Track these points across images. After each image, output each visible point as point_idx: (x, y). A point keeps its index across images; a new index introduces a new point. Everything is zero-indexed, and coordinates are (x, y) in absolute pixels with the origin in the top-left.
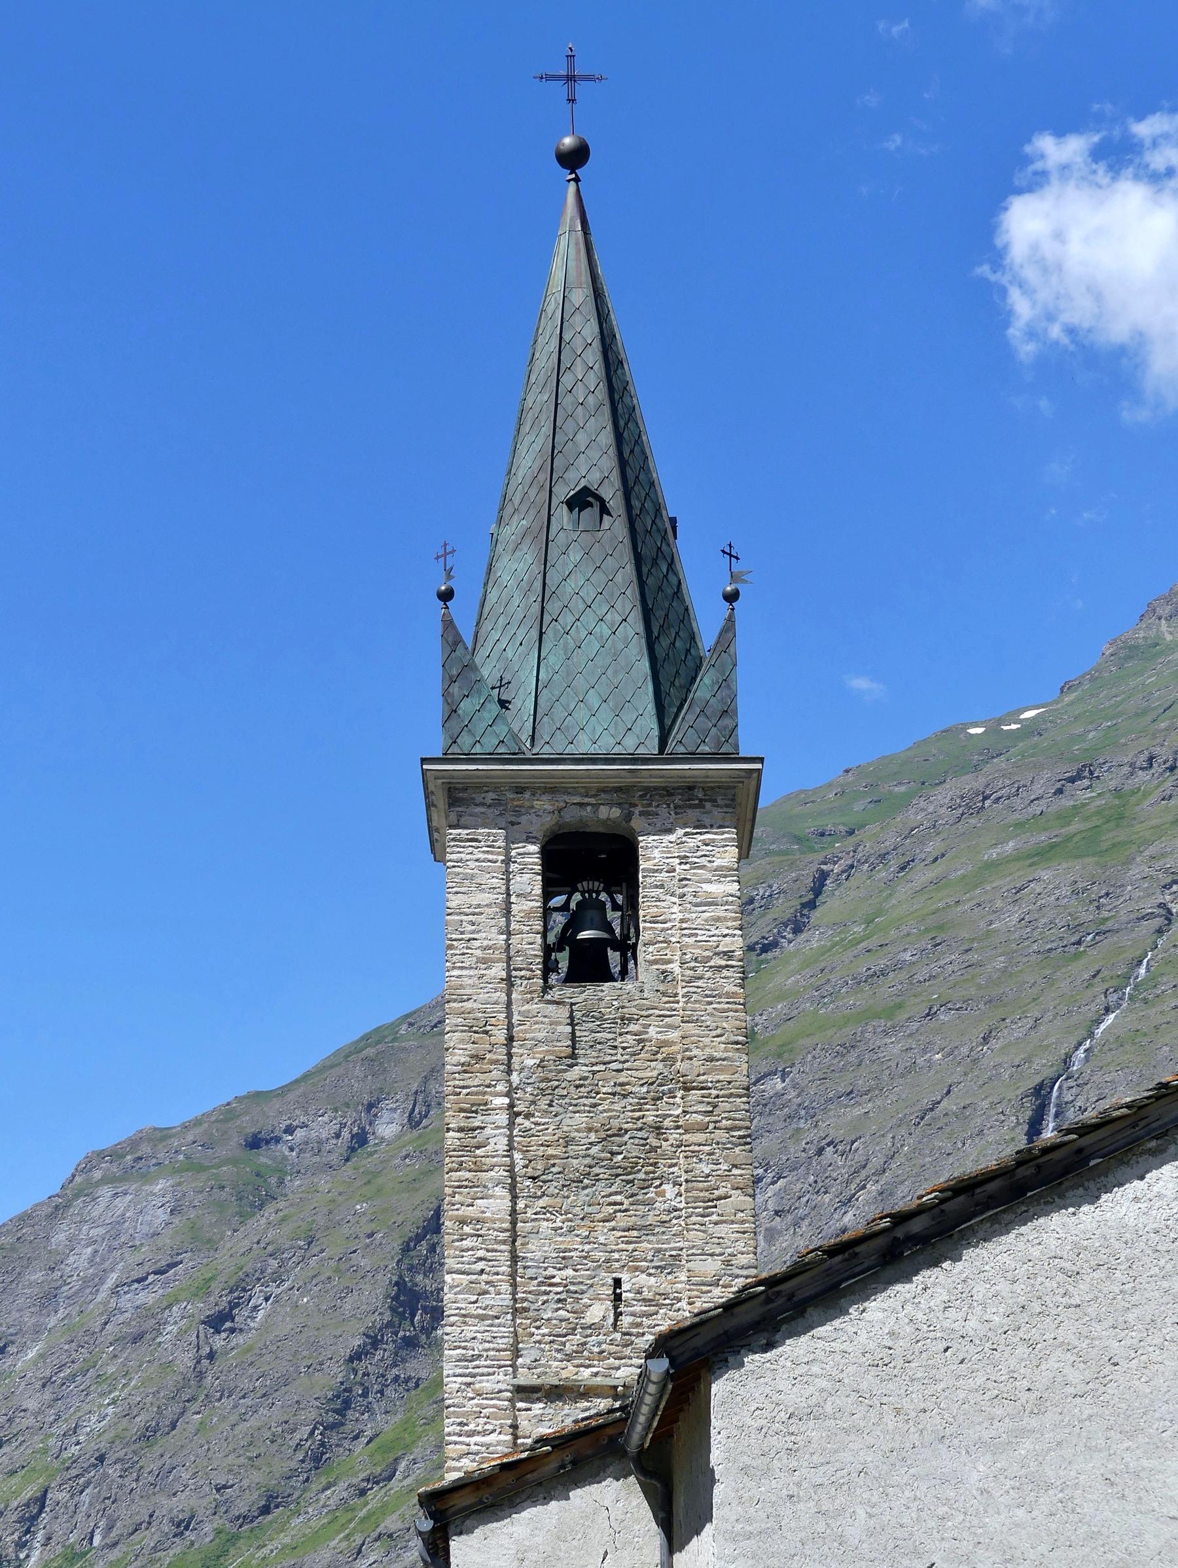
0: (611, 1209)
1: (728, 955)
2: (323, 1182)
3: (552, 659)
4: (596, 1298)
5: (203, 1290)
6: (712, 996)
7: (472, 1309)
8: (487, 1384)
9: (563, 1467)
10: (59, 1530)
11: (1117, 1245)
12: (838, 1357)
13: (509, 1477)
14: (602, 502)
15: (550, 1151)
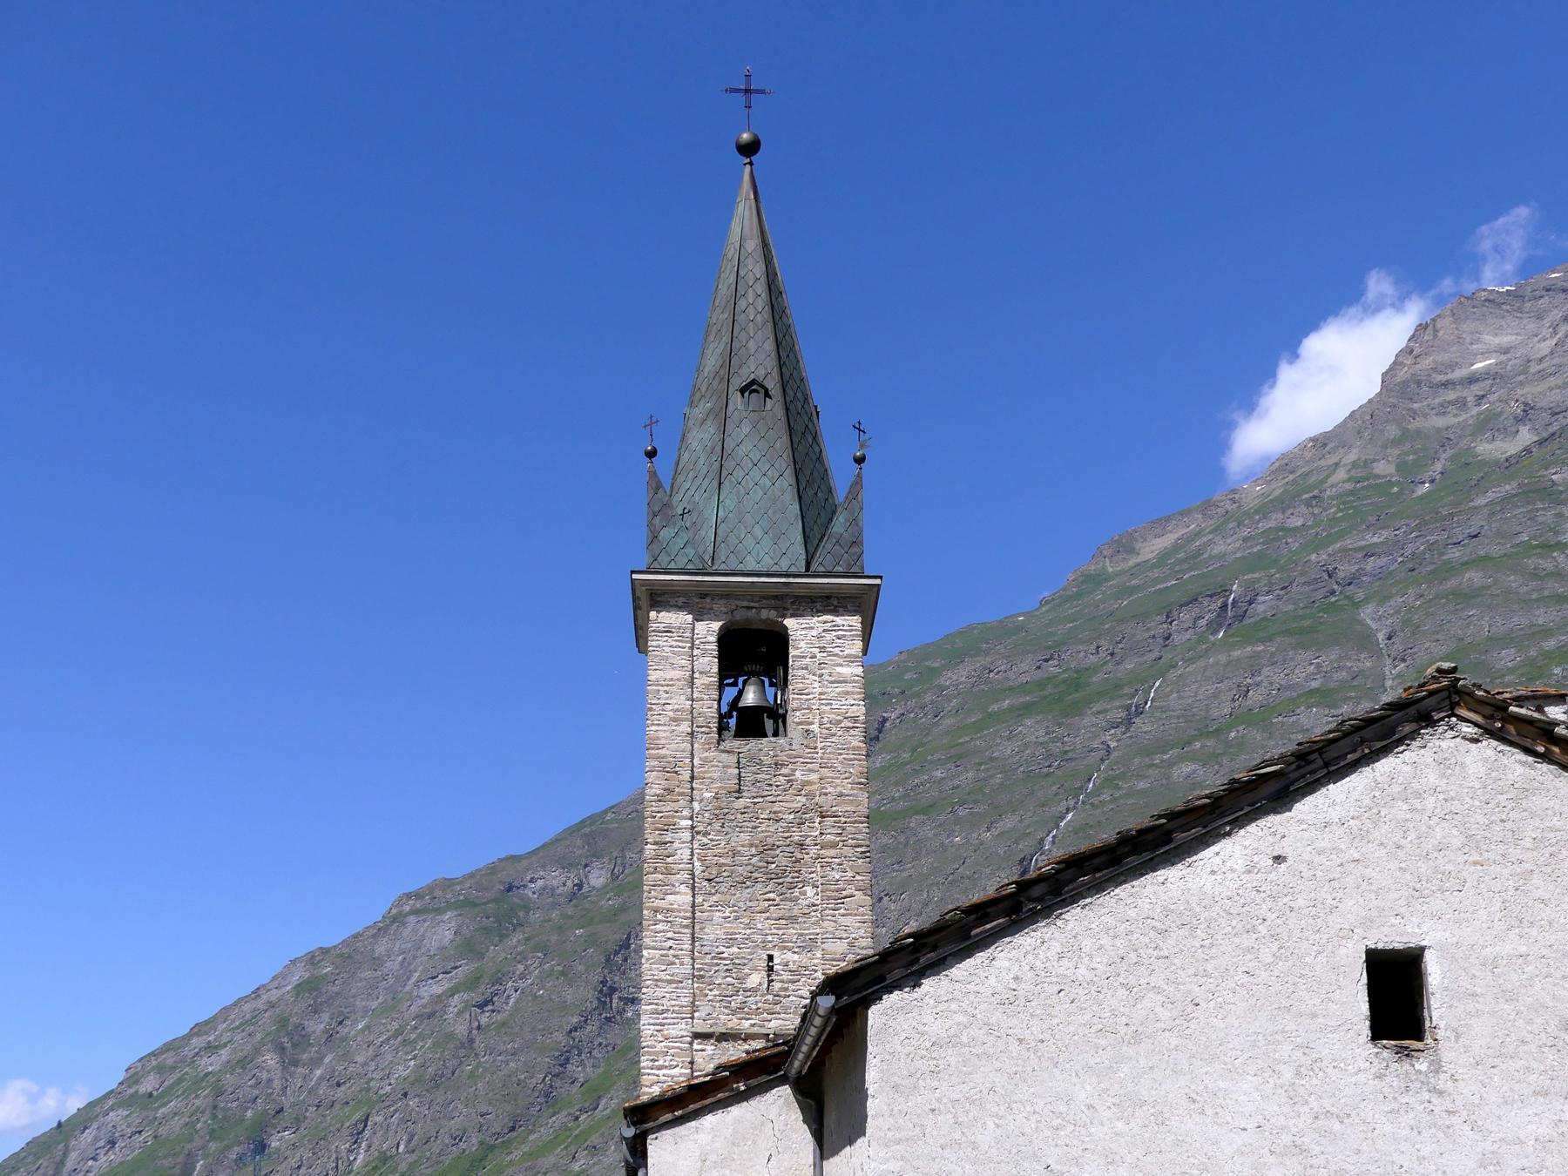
0: (766, 904)
1: (855, 719)
3: (728, 502)
4: (755, 969)
7: (663, 976)
8: (672, 1031)
11: (1198, 909)
12: (972, 997)
14: (766, 391)
15: (722, 861)
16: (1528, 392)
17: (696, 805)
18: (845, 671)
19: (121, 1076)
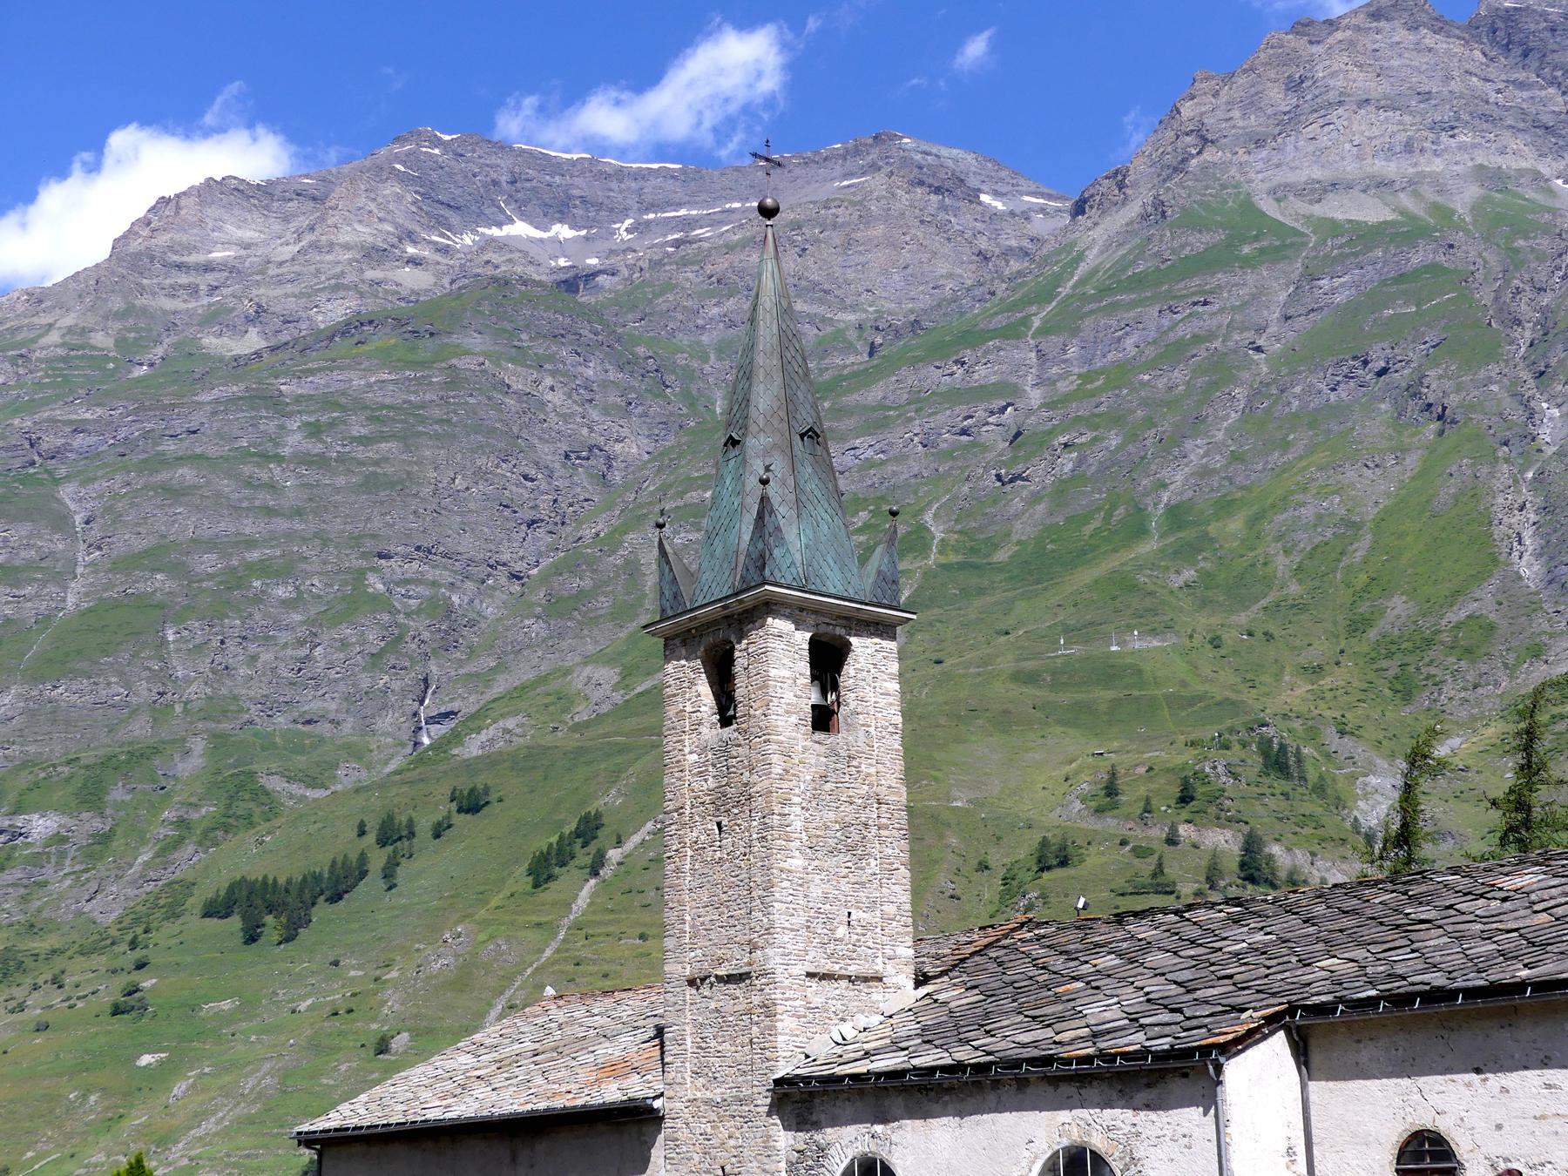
7: (787, 925)
16: (265, 293)
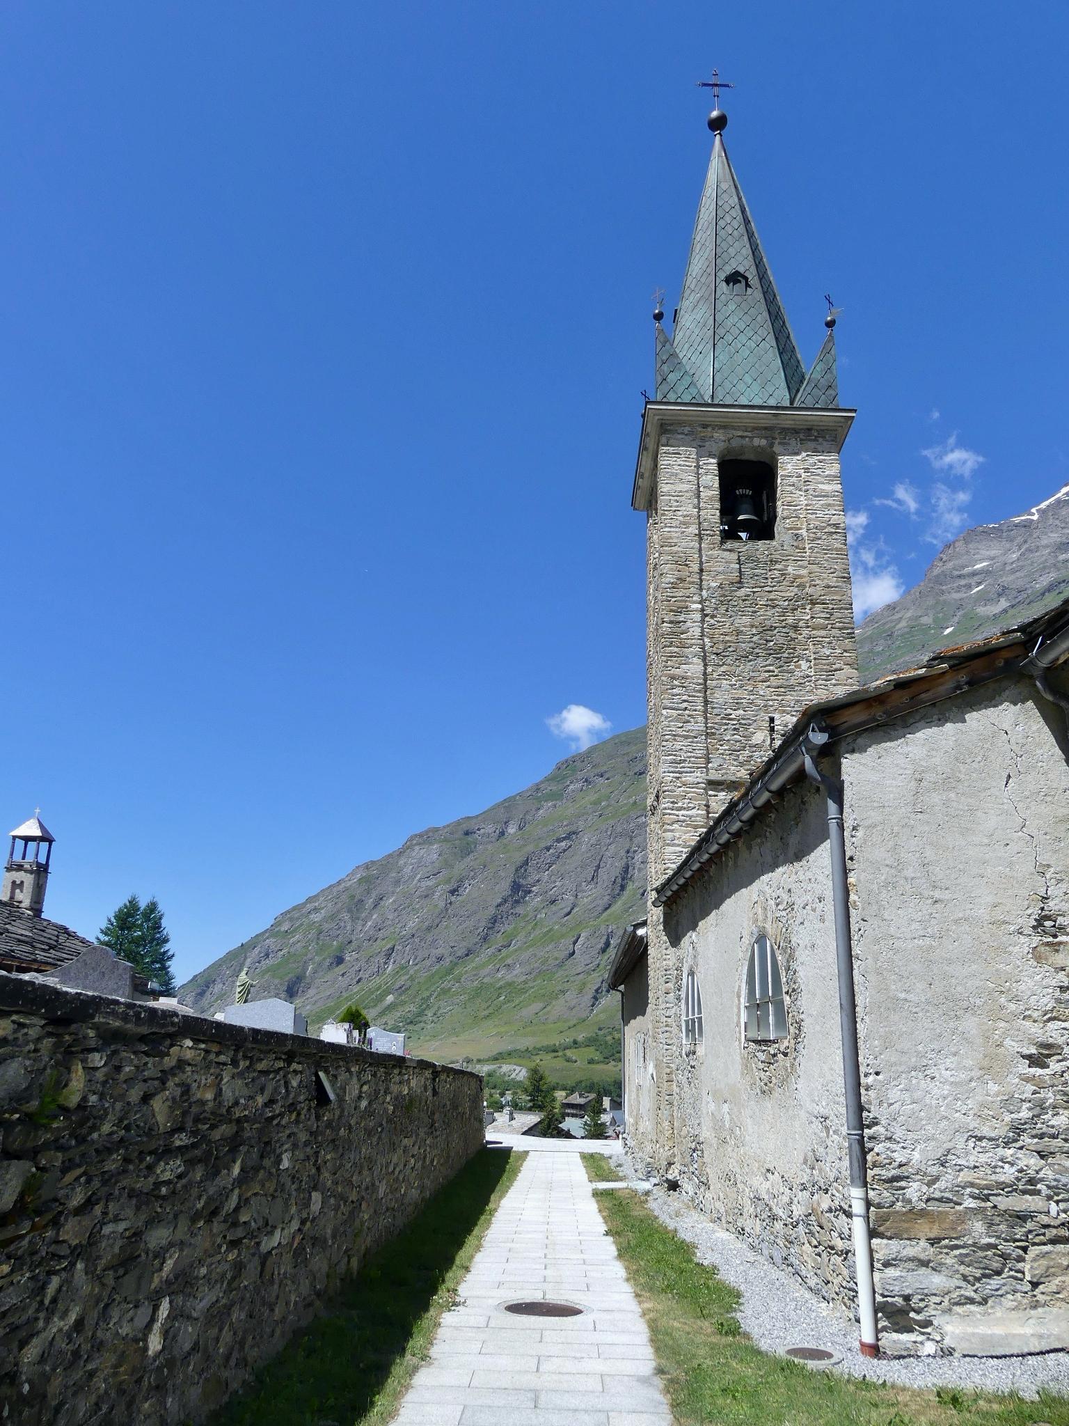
0: (767, 675)
2: (489, 847)
3: (721, 357)
4: (759, 728)
5: (448, 881)
6: (828, 550)
7: (680, 731)
8: (689, 778)
9: (959, 687)
10: (398, 958)
13: (903, 697)
14: (746, 279)
15: (727, 638)
16: (1007, 580)
17: (704, 593)
18: (827, 487)
19: (272, 922)
